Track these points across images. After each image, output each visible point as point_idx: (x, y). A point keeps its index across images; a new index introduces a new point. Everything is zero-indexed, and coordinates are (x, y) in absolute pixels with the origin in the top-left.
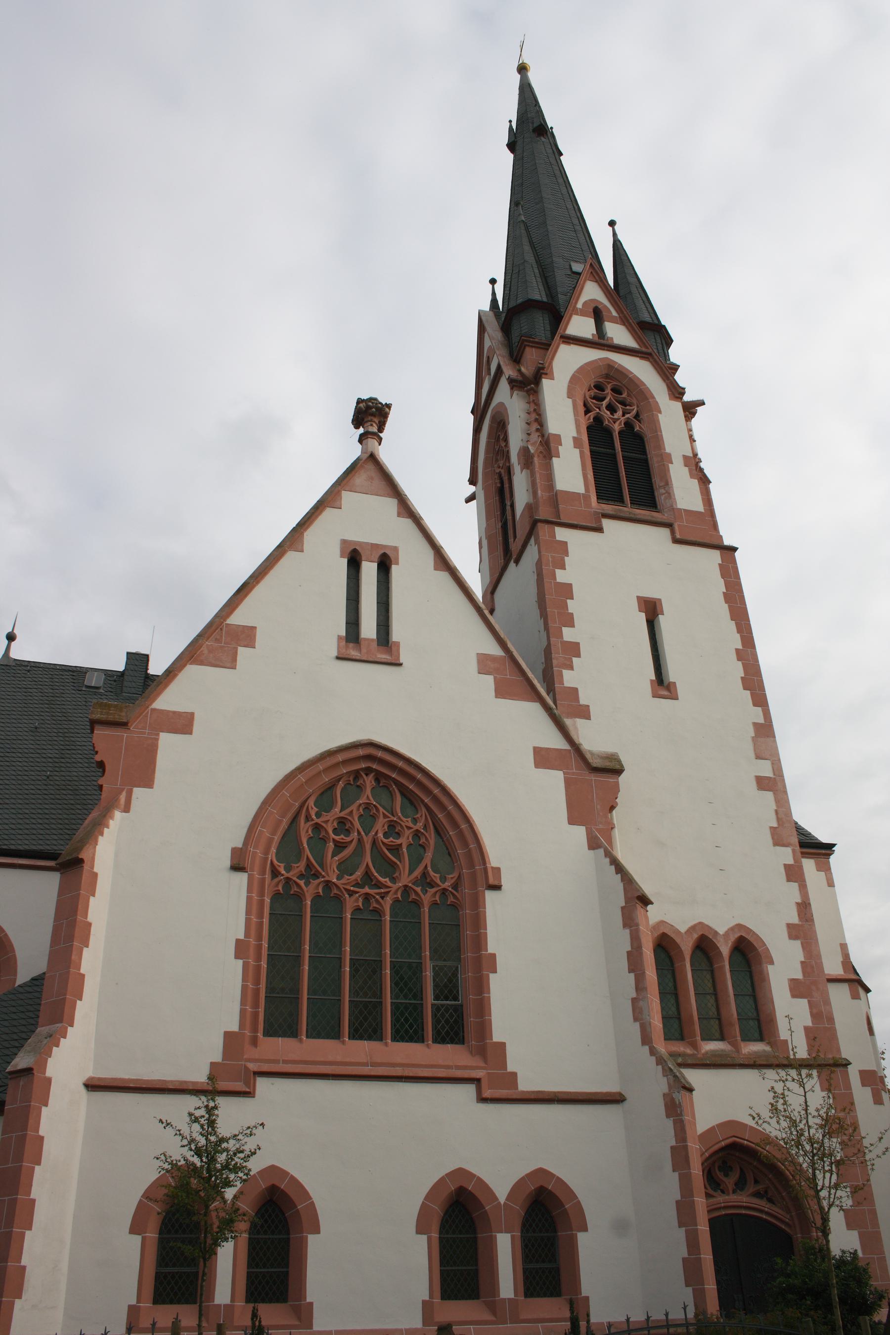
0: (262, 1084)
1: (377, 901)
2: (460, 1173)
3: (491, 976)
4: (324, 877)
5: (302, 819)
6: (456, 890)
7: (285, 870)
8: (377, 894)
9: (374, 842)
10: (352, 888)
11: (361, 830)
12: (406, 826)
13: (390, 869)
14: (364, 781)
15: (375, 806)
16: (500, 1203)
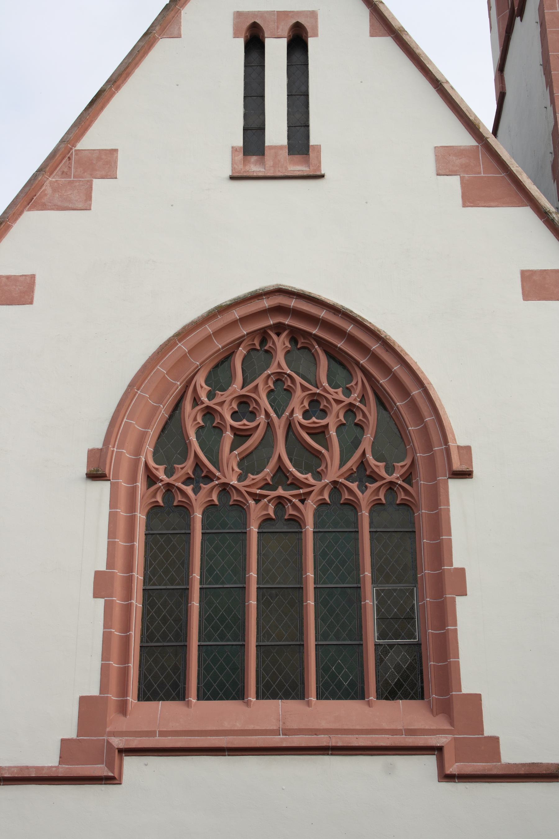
1: (294, 506)
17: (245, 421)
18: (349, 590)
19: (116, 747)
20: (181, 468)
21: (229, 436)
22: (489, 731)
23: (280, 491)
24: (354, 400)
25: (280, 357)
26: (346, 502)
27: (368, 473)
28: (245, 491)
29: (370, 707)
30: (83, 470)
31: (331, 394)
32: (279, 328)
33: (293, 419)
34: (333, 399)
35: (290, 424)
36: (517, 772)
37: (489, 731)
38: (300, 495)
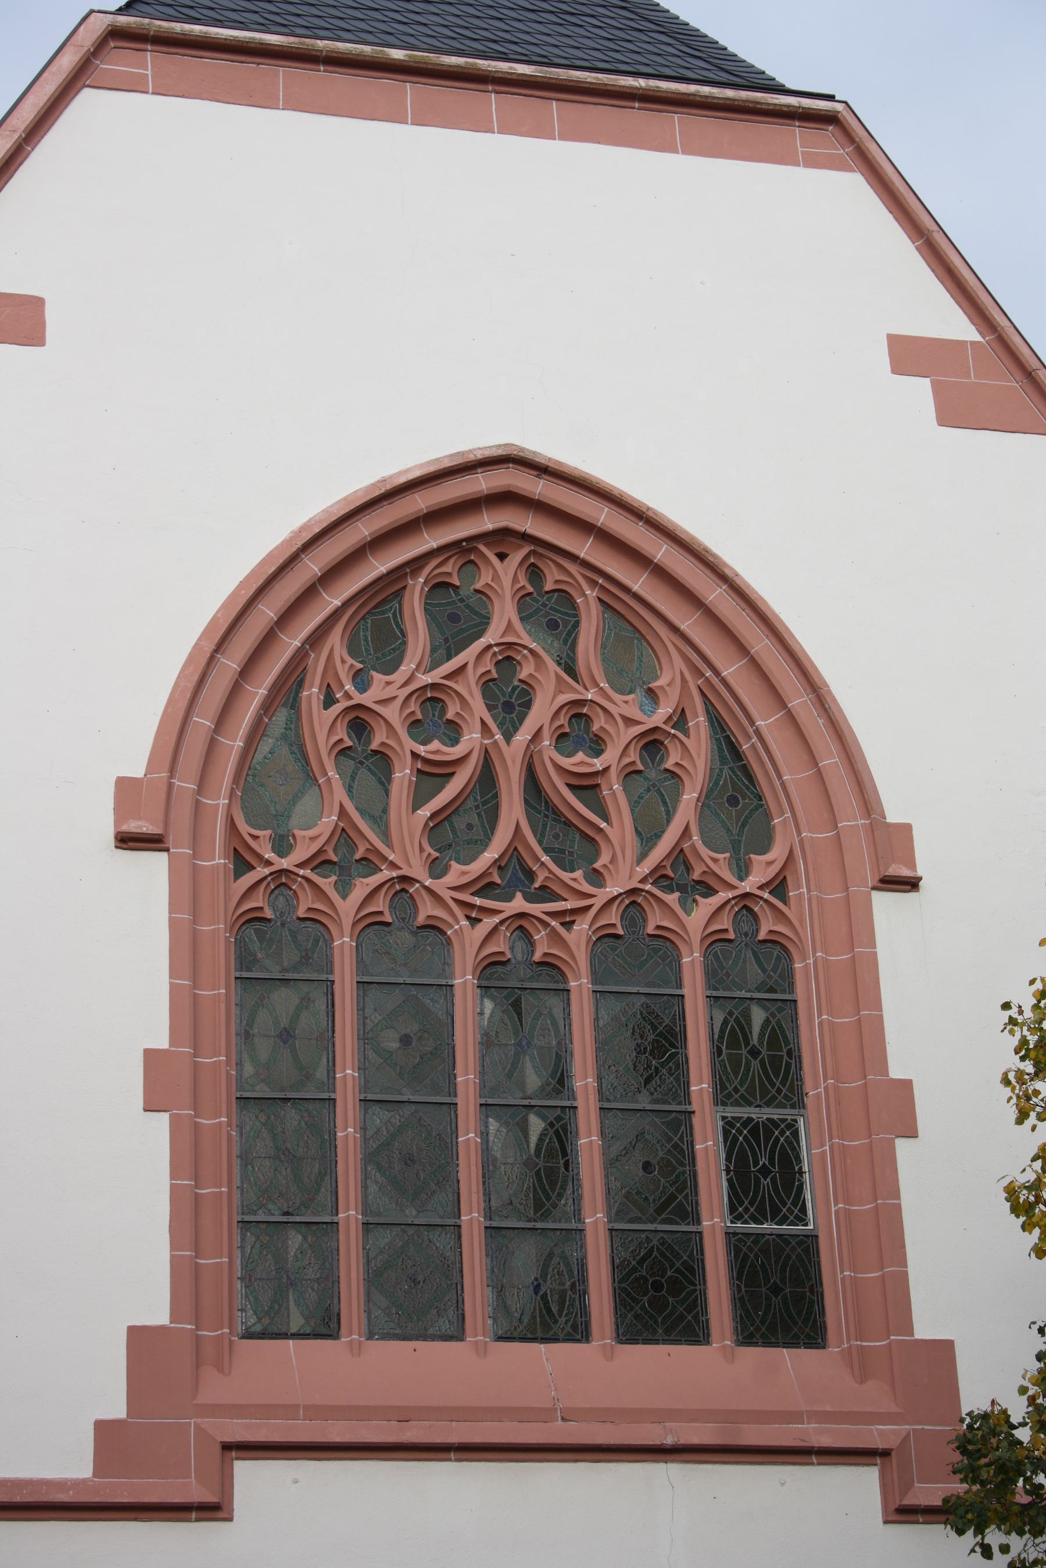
1: (554, 935)
3: (162, 1042)
4: (393, 865)
5: (312, 693)
6: (785, 900)
7: (274, 850)
8: (552, 914)
10: (478, 901)
14: (496, 576)
15: (531, 651)
18: (413, 1107)
19: (220, 1440)
20: (310, 838)
21: (403, 774)
23: (518, 904)
24: (664, 723)
26: (428, 923)
27: (696, 875)
28: (452, 898)
31: (615, 703)
33: (540, 751)
34: (620, 715)
36: (658, 1442)
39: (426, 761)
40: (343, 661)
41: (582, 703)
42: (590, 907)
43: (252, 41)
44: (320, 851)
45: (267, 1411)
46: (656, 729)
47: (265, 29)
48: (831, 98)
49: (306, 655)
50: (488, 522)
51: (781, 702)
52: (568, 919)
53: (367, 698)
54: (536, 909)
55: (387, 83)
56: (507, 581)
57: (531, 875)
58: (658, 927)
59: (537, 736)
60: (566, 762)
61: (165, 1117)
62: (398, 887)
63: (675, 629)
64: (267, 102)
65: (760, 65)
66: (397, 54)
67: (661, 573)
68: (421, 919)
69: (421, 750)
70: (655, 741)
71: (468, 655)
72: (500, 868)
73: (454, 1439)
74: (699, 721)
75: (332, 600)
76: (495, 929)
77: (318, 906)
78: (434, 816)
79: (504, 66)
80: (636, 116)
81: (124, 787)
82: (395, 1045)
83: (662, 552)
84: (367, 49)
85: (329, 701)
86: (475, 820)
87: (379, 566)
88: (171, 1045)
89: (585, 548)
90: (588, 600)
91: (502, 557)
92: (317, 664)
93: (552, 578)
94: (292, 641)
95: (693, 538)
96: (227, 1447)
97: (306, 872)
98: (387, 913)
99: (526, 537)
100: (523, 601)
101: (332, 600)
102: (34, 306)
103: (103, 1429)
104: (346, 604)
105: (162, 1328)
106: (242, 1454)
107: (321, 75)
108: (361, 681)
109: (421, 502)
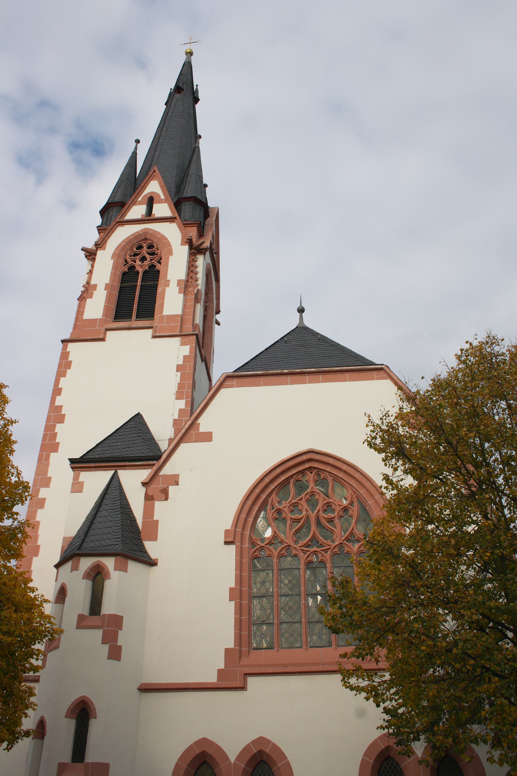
0: (251, 680)
1: (323, 555)
2: (261, 740)
4: (286, 543)
9: (318, 518)
10: (305, 549)
11: (308, 509)
12: (338, 505)
13: (329, 533)
16: (231, 762)
17: (296, 515)
22: (119, 643)
25: (311, 484)
29: (59, 647)
30: (222, 540)
32: (310, 469)
35: (318, 517)
37: (119, 643)
38: (325, 550)
39: (294, 519)
40: (275, 499)
41: (329, 502)
42: (331, 548)
43: (255, 374)
44: (270, 541)
45: (254, 666)
46: (346, 507)
47: (259, 371)
48: (383, 365)
49: (268, 499)
50: (307, 466)
51: (373, 497)
52: (326, 551)
53: (281, 507)
54: (318, 549)
55: (284, 377)
56: (312, 478)
57: (318, 542)
58: (347, 551)
59: (319, 511)
60: (325, 516)
61: (234, 602)
62: (288, 547)
63: (349, 484)
64: (259, 385)
65: (371, 360)
66: (286, 371)
67: (345, 472)
68: (293, 554)
69: (293, 517)
70: (346, 509)
71: (303, 495)
72: (311, 541)
73: (296, 670)
74: (356, 503)
75: (273, 487)
76: (309, 555)
77: (270, 553)
78: (295, 531)
79: (309, 370)
80: (339, 375)
81: (227, 531)
82: (287, 583)
83: (345, 467)
84: (279, 371)
85: (273, 508)
86: (305, 531)
87: (283, 478)
88: (235, 586)
89: (329, 469)
90: (330, 479)
91: (311, 473)
92: (270, 500)
93: (322, 476)
94: (264, 496)
95: (351, 463)
96: (245, 674)
97: (268, 546)
98: (285, 553)
99: (315, 468)
100: (316, 481)
101: (273, 487)
102: (211, 433)
103: (219, 671)
104: (276, 487)
105: (232, 648)
106: (250, 676)
107: (270, 378)
108: (279, 502)
109: (291, 463)
